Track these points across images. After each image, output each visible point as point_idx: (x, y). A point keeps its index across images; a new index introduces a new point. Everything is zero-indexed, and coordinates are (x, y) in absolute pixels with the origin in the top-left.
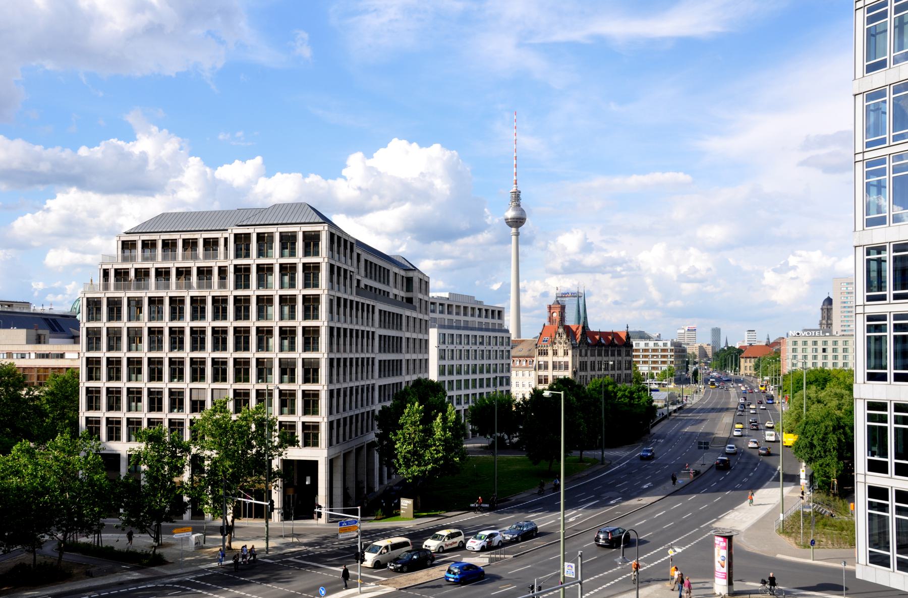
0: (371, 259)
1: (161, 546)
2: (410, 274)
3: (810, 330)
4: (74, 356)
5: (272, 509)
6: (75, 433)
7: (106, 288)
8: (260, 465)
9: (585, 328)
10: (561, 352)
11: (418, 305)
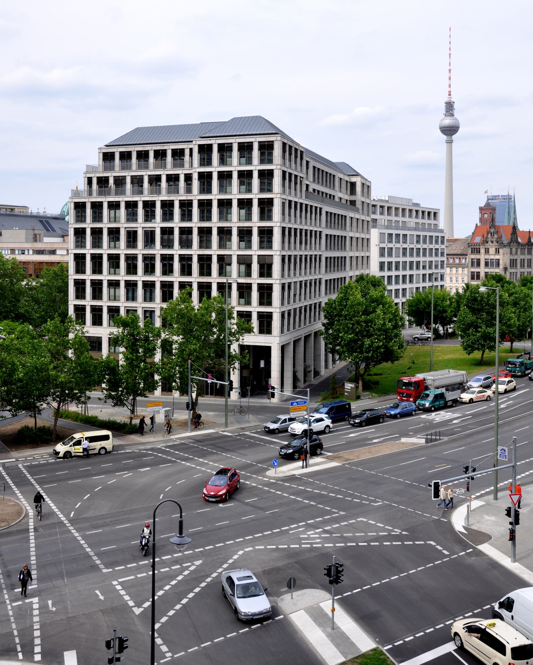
0: (318, 165)
2: (353, 179)
4: (65, 251)
5: (231, 388)
6: (64, 315)
7: (90, 194)
8: (220, 350)
9: (515, 228)
10: (492, 250)
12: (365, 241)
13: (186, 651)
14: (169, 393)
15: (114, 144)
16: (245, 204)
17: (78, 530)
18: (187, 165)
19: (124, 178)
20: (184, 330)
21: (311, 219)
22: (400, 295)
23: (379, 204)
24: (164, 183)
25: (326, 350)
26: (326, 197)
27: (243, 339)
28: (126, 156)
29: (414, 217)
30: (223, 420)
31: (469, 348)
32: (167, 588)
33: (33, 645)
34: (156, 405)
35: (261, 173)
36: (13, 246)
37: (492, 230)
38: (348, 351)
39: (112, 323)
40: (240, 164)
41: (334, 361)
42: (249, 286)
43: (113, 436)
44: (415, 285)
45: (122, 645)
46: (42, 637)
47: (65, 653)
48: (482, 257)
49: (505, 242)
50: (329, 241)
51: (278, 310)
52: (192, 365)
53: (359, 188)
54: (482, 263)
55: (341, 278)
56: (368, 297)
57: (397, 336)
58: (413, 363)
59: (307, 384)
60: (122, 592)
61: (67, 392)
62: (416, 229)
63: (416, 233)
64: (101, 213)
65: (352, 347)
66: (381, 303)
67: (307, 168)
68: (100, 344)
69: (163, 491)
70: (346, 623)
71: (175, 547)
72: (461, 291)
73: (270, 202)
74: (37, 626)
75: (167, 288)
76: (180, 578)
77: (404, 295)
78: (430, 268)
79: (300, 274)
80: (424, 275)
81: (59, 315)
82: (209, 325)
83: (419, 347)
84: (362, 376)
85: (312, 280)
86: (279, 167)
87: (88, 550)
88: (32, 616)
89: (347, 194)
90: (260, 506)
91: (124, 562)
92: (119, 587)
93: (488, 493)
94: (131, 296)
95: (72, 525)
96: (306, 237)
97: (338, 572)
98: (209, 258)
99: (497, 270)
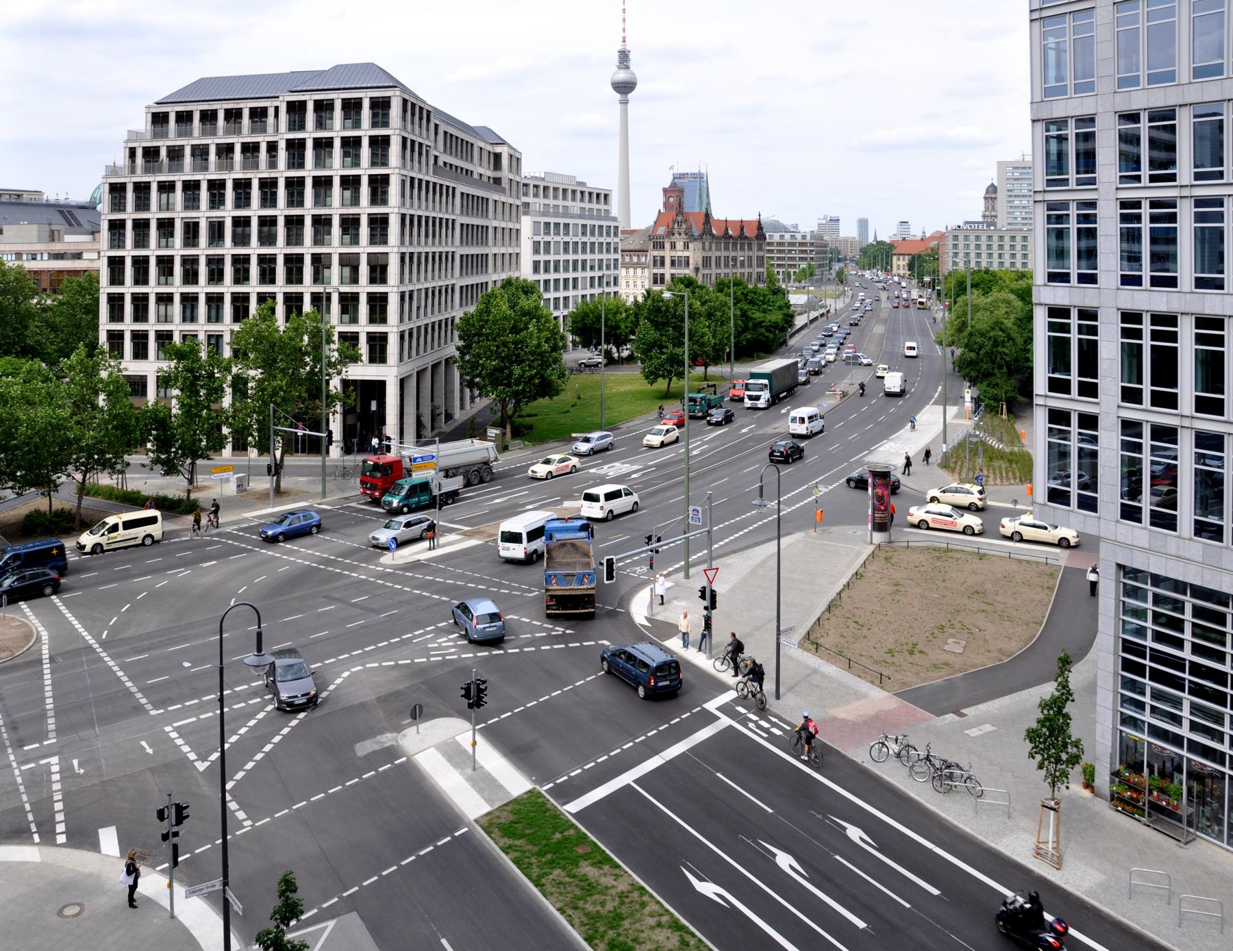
0: (451, 130)
1: (199, 489)
2: (498, 149)
3: (973, 223)
4: (94, 255)
5: (330, 442)
6: (93, 346)
7: (133, 170)
8: (315, 388)
9: (708, 215)
10: (680, 245)
11: (507, 187)
12: (514, 233)
13: (272, 816)
16: (350, 183)
17: (113, 657)
18: (270, 129)
19: (182, 148)
20: (264, 360)
22: (561, 305)
23: (532, 183)
24: (238, 155)
28: (184, 118)
30: (319, 488)
31: (652, 376)
32: (243, 731)
33: (53, 823)
34: (225, 471)
35: (374, 141)
36: (19, 248)
37: (679, 219)
38: (491, 383)
39: (162, 355)
40: (344, 128)
41: (472, 399)
42: (355, 297)
43: (163, 519)
44: (580, 292)
45: (181, 814)
46: (66, 810)
47: (100, 831)
48: (667, 254)
49: (696, 234)
51: (395, 329)
52: (275, 411)
53: (505, 161)
54: (668, 262)
56: (517, 308)
57: (556, 361)
59: (436, 431)
60: (179, 742)
62: (581, 216)
63: (581, 222)
64: (148, 199)
65: (497, 379)
66: (534, 317)
69: (234, 594)
70: (492, 760)
71: (252, 670)
72: (640, 299)
73: (385, 179)
74: (58, 796)
75: (240, 302)
76: (261, 716)
77: (566, 306)
78: (600, 268)
79: (426, 279)
80: (592, 278)
81: (86, 346)
82: (302, 353)
83: (586, 376)
84: (510, 417)
86: (397, 132)
87: (129, 684)
88: (50, 782)
90: (373, 606)
91: (181, 699)
92: (174, 735)
93: (677, 571)
94: (189, 314)
95: (105, 651)
96: (433, 227)
97: (480, 691)
98: (300, 258)
99: (687, 271)
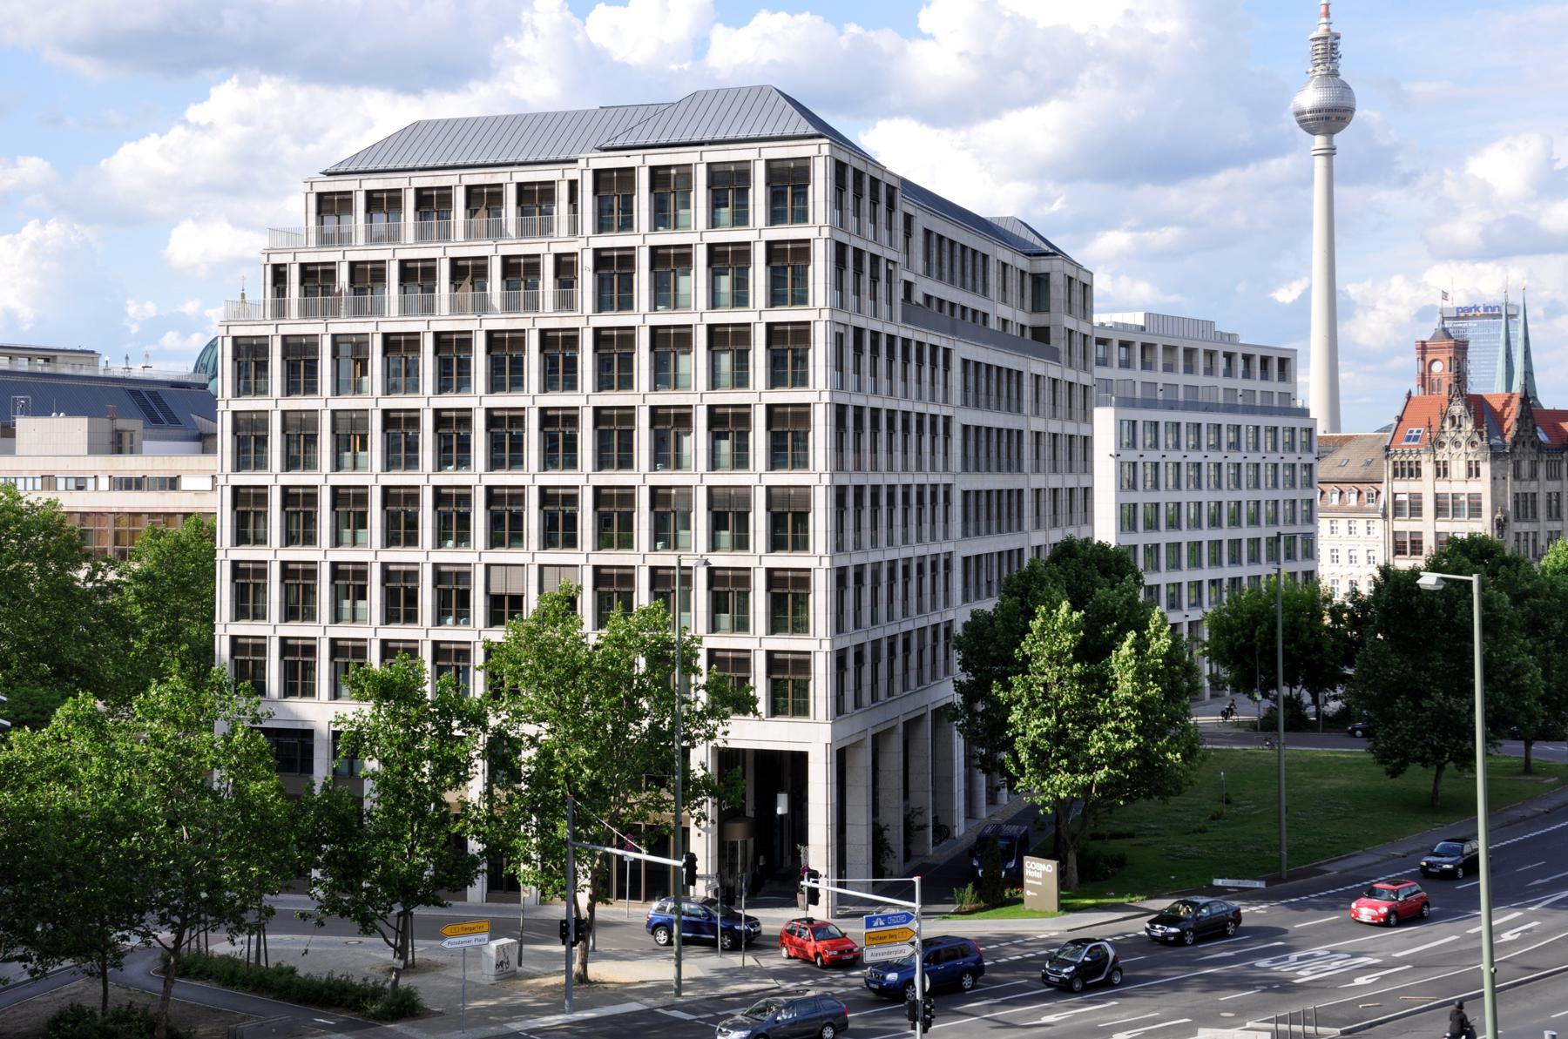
2: (1043, 266)
4: (202, 483)
5: (692, 878)
7: (280, 312)
8: (659, 762)
9: (1528, 399)
10: (1458, 468)
14: (511, 894)
15: (351, 168)
21: (919, 381)
25: (968, 764)
26: (963, 317)
27: (726, 733)
29: (1221, 373)
31: (1394, 759)
34: (471, 931)
36: (47, 466)
41: (992, 799)
50: (972, 443)
53: (1057, 292)
54: (1428, 506)
55: (1010, 552)
58: (1228, 802)
59: (913, 863)
61: (204, 895)
67: (908, 234)
68: (308, 752)
72: (1366, 589)
77: (1198, 603)
85: (924, 557)
89: (1022, 308)
